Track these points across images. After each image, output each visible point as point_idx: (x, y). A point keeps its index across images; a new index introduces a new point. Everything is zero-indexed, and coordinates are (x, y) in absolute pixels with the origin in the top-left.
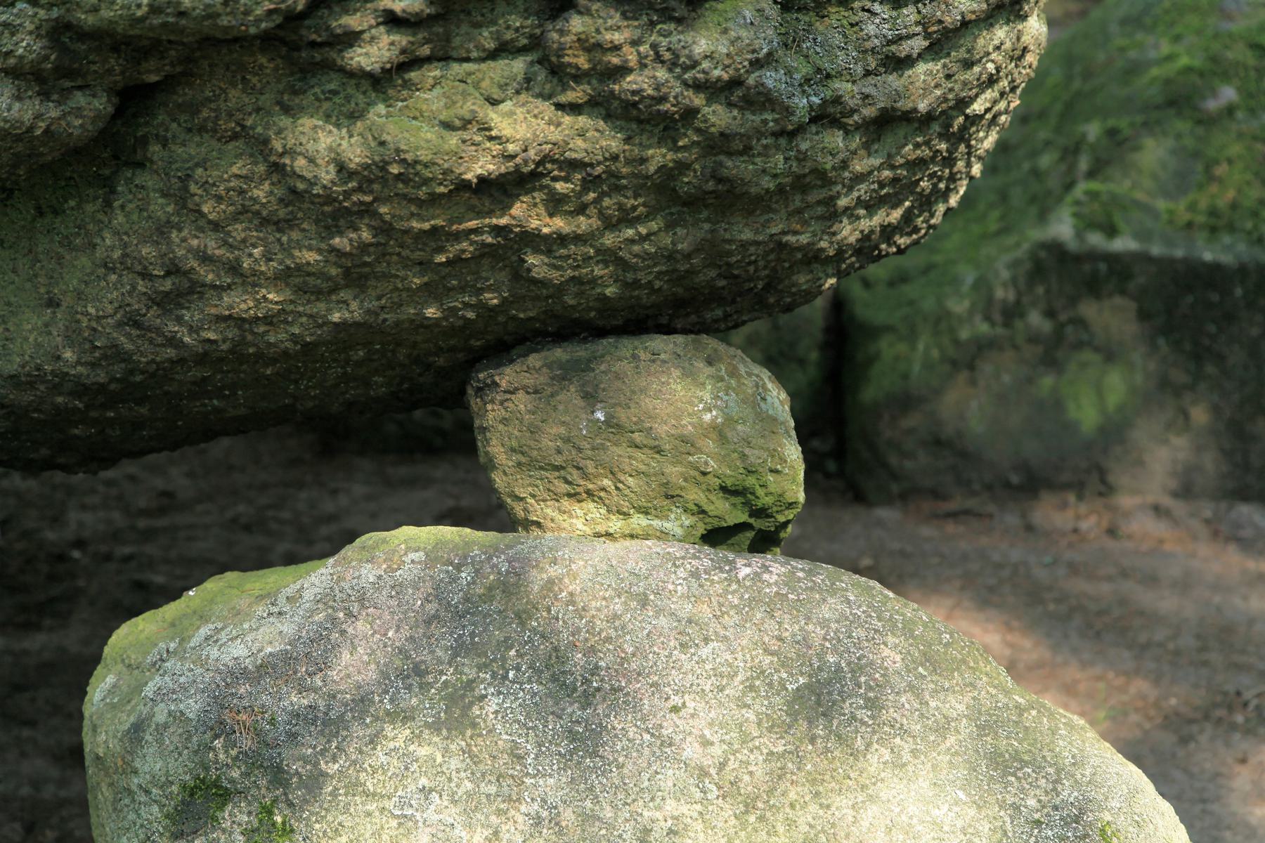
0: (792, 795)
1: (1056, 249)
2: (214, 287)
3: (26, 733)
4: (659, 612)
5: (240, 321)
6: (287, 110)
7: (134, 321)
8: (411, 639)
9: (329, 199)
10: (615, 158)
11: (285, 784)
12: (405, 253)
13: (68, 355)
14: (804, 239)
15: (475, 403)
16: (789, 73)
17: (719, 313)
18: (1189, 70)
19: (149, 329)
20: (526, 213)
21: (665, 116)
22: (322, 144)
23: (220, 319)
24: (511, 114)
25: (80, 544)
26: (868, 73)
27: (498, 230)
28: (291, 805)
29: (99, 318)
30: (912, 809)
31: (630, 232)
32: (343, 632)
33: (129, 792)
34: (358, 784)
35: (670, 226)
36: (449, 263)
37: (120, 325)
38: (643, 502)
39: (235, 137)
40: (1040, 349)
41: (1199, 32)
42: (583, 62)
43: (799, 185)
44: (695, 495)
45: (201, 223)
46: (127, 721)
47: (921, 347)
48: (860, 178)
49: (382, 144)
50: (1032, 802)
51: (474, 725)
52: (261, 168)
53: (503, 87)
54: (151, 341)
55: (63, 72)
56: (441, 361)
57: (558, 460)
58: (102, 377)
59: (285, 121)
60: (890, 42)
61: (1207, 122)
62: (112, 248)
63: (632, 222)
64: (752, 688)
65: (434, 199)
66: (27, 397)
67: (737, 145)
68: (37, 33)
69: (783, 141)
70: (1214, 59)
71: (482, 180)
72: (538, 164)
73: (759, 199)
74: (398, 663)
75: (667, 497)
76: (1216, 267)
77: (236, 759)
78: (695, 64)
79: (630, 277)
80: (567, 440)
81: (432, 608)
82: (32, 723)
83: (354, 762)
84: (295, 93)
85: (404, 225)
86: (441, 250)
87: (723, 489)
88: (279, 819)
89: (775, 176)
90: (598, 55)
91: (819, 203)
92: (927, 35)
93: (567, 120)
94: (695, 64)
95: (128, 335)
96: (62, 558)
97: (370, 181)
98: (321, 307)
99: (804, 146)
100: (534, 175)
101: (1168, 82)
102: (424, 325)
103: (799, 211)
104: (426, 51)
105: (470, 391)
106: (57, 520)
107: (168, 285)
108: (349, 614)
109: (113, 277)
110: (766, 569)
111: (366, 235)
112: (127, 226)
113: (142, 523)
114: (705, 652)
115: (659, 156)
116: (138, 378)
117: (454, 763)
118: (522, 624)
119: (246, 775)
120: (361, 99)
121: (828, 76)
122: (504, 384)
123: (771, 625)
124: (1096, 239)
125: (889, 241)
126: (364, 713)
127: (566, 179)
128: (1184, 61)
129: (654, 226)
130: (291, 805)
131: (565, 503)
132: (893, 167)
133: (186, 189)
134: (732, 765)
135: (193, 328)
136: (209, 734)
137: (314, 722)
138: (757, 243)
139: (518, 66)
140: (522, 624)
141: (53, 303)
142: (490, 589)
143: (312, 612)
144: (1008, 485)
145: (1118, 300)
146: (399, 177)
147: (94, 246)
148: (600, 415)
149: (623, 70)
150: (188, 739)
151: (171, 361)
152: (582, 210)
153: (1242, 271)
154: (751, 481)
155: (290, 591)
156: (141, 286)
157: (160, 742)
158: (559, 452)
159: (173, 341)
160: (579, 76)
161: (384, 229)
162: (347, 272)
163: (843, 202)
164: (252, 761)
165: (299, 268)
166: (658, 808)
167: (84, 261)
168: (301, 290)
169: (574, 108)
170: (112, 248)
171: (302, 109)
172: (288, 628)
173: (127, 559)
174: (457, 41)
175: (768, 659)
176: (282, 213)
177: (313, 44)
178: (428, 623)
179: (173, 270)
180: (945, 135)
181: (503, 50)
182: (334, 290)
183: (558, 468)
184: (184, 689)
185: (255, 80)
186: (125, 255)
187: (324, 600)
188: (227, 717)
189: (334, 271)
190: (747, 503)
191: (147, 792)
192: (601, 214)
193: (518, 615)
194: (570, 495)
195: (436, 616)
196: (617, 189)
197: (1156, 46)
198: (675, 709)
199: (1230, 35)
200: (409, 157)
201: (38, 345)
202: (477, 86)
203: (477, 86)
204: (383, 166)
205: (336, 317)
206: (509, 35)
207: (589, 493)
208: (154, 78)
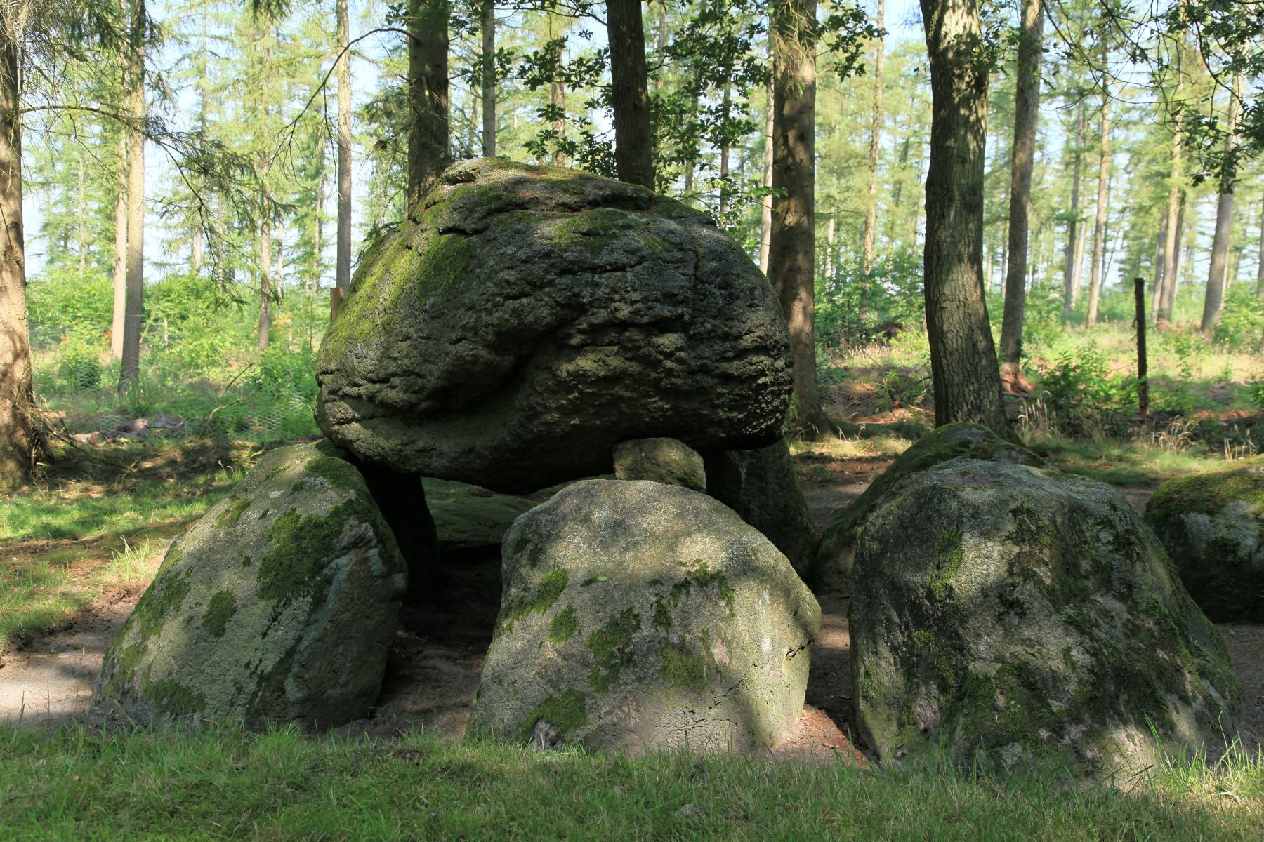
20: (619, 390)
22: (566, 368)
27: (612, 395)
135: (536, 427)
139: (616, 348)
149: (640, 348)
159: (532, 431)
160: (630, 349)
161: (580, 392)
179: (531, 408)
181: (610, 343)
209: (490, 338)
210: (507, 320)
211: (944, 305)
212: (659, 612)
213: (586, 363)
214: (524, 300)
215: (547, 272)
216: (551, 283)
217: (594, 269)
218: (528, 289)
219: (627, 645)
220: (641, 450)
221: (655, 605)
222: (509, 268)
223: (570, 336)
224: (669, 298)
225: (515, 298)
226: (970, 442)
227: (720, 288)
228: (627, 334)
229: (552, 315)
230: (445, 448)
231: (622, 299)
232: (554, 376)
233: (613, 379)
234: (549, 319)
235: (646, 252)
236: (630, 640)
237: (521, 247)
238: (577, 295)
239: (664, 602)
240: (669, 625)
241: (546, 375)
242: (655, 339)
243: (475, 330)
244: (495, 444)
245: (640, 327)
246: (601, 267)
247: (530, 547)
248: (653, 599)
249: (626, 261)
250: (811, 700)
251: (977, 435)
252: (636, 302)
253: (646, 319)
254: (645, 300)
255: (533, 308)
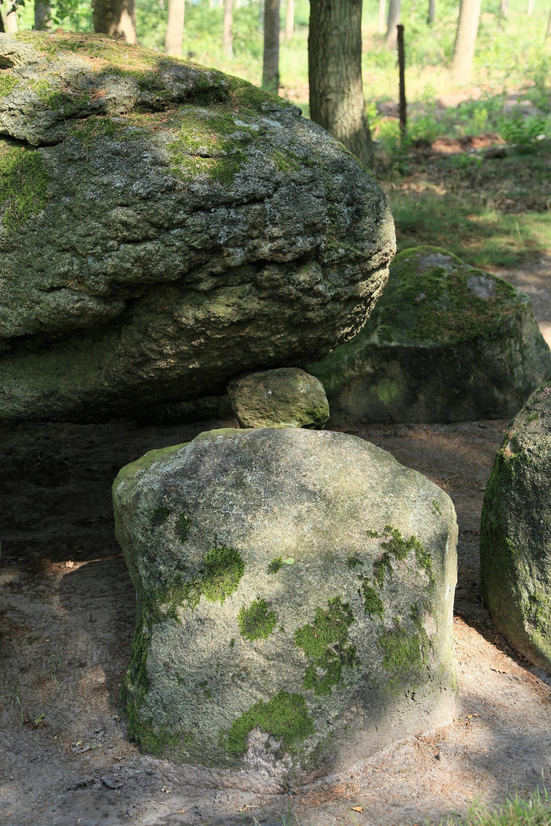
0: (342, 498)
1: (373, 346)
2: (154, 359)
3: (62, 517)
4: (296, 448)
5: (161, 369)
6: (178, 304)
7: (128, 372)
8: (222, 461)
9: (192, 329)
10: (276, 313)
11: (187, 507)
12: (213, 345)
13: (106, 384)
14: (327, 336)
15: (230, 392)
16: (325, 286)
17: (299, 361)
18: (410, 289)
19: (133, 374)
21: (292, 300)
22: (190, 315)
23: (155, 369)
24: (246, 301)
25: (67, 459)
26: (346, 285)
27: (241, 337)
28: (190, 513)
29: (116, 372)
30: (378, 500)
31: (279, 336)
32: (201, 461)
33: (136, 514)
34: (210, 505)
35: (290, 334)
36: (226, 348)
37: (124, 373)
38: (284, 418)
39: (162, 313)
40: (370, 378)
41: (411, 277)
42: (267, 285)
43: (327, 320)
44: (299, 415)
45: (151, 340)
46: (133, 493)
47: (332, 380)
48: (343, 317)
49: (209, 312)
50: (412, 496)
51: (244, 485)
52: (170, 322)
53: (243, 293)
54: (133, 378)
55: (112, 296)
56: (218, 380)
57: (258, 407)
58: (116, 390)
59: (178, 307)
60: (352, 276)
61: (416, 305)
62: (121, 350)
63: (279, 333)
64: (326, 468)
65: (224, 328)
66: (91, 398)
67: (311, 308)
68: (105, 284)
69: (323, 306)
70: (418, 285)
71: (238, 321)
72: (254, 316)
73: (315, 324)
74: (218, 468)
75: (291, 416)
76: (424, 349)
77: (171, 501)
78: (301, 283)
79: (278, 350)
80: (260, 401)
81: (227, 452)
82: (63, 514)
83: (208, 499)
84: (181, 298)
85: (214, 336)
86: (224, 344)
87: (307, 413)
88: (186, 518)
89: (321, 317)
90: (272, 282)
91: (331, 325)
92: (362, 273)
93: (262, 302)
94: (301, 283)
95: (126, 377)
96: (62, 463)
97: (204, 324)
98: (187, 363)
99: (329, 308)
100: (252, 319)
101: (403, 293)
102: (216, 368)
103: (325, 328)
104: (221, 283)
105: (228, 388)
106: (58, 452)
107: (140, 359)
108: (202, 455)
109: (122, 359)
110: (327, 434)
111: (202, 340)
112: (127, 342)
113: (86, 451)
114: (311, 459)
115: (289, 312)
116: (128, 390)
117: (240, 496)
118: (255, 454)
119: (175, 505)
120: (201, 299)
121: (336, 286)
122: (240, 385)
123: (330, 450)
124: (386, 343)
125: (346, 338)
126: (210, 484)
127: (262, 320)
128: (408, 286)
129: (286, 334)
130: (190, 513)
131: (260, 420)
132: (351, 314)
133: (147, 330)
134: (323, 491)
135: (147, 373)
136: (162, 495)
137: (195, 488)
138: (314, 338)
139: (247, 287)
140: (255, 454)
141: (100, 368)
142: (245, 445)
143: (190, 456)
144: (362, 423)
145: (394, 361)
146: (213, 322)
147: (115, 350)
148: (270, 393)
149: (280, 286)
150: (156, 496)
151: (139, 384)
152: (266, 330)
153: (432, 350)
154: (315, 410)
155: (181, 450)
156: (131, 360)
157: (146, 498)
158: (258, 404)
159: (140, 377)
160: (265, 289)
161: (208, 338)
162: (195, 352)
163: (338, 325)
164: (177, 501)
165: (181, 352)
166: (303, 505)
167: (111, 355)
168: (180, 359)
169: (264, 299)
170: (121, 350)
171: (183, 303)
172: (183, 461)
173: (84, 462)
174: (230, 280)
175: (330, 460)
176: (176, 335)
177: (188, 283)
178: (227, 456)
179: (142, 354)
180: (365, 305)
181: (243, 282)
182: (191, 358)
183: (257, 409)
184: (152, 481)
185: (168, 295)
186: (126, 351)
187: (194, 451)
188: (167, 488)
189: (191, 352)
190: (314, 417)
191: (143, 514)
192: (271, 331)
193: (254, 452)
194: (261, 417)
195: (229, 454)
196: (276, 323)
197: (398, 282)
198: (304, 476)
199: (421, 277)
200: (217, 315)
201: (96, 382)
202: (236, 293)
203: (236, 293)
204: (209, 319)
205: (191, 367)
206: (245, 278)
207: (267, 416)
208: (137, 296)
209: (102, 288)
210: (128, 270)
211: (329, 97)
212: (368, 597)
213: (222, 309)
214: (149, 246)
215: (175, 211)
216: (181, 224)
217: (229, 204)
218: (152, 232)
219: (344, 641)
220: (267, 387)
221: (362, 590)
222: (122, 205)
223: (200, 281)
224: (312, 229)
225: (136, 242)
226: (442, 271)
227: (348, 204)
228: (266, 273)
229: (183, 262)
230: (17, 392)
231: (262, 236)
232: (176, 322)
233: (248, 321)
234: (182, 267)
235: (279, 176)
236: (346, 634)
237: (134, 178)
238: (213, 237)
239: (370, 584)
240: (381, 609)
241: (161, 321)
242: (295, 276)
243: (81, 280)
244: (87, 389)
245: (280, 265)
246: (237, 200)
247: (173, 519)
248: (359, 583)
249: (263, 191)
250: (456, 614)
251: (444, 262)
252: (277, 238)
253: (289, 257)
254: (286, 236)
255: (163, 256)
